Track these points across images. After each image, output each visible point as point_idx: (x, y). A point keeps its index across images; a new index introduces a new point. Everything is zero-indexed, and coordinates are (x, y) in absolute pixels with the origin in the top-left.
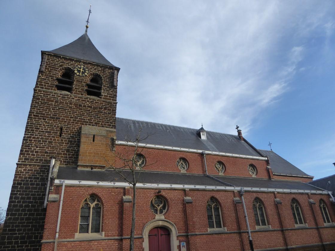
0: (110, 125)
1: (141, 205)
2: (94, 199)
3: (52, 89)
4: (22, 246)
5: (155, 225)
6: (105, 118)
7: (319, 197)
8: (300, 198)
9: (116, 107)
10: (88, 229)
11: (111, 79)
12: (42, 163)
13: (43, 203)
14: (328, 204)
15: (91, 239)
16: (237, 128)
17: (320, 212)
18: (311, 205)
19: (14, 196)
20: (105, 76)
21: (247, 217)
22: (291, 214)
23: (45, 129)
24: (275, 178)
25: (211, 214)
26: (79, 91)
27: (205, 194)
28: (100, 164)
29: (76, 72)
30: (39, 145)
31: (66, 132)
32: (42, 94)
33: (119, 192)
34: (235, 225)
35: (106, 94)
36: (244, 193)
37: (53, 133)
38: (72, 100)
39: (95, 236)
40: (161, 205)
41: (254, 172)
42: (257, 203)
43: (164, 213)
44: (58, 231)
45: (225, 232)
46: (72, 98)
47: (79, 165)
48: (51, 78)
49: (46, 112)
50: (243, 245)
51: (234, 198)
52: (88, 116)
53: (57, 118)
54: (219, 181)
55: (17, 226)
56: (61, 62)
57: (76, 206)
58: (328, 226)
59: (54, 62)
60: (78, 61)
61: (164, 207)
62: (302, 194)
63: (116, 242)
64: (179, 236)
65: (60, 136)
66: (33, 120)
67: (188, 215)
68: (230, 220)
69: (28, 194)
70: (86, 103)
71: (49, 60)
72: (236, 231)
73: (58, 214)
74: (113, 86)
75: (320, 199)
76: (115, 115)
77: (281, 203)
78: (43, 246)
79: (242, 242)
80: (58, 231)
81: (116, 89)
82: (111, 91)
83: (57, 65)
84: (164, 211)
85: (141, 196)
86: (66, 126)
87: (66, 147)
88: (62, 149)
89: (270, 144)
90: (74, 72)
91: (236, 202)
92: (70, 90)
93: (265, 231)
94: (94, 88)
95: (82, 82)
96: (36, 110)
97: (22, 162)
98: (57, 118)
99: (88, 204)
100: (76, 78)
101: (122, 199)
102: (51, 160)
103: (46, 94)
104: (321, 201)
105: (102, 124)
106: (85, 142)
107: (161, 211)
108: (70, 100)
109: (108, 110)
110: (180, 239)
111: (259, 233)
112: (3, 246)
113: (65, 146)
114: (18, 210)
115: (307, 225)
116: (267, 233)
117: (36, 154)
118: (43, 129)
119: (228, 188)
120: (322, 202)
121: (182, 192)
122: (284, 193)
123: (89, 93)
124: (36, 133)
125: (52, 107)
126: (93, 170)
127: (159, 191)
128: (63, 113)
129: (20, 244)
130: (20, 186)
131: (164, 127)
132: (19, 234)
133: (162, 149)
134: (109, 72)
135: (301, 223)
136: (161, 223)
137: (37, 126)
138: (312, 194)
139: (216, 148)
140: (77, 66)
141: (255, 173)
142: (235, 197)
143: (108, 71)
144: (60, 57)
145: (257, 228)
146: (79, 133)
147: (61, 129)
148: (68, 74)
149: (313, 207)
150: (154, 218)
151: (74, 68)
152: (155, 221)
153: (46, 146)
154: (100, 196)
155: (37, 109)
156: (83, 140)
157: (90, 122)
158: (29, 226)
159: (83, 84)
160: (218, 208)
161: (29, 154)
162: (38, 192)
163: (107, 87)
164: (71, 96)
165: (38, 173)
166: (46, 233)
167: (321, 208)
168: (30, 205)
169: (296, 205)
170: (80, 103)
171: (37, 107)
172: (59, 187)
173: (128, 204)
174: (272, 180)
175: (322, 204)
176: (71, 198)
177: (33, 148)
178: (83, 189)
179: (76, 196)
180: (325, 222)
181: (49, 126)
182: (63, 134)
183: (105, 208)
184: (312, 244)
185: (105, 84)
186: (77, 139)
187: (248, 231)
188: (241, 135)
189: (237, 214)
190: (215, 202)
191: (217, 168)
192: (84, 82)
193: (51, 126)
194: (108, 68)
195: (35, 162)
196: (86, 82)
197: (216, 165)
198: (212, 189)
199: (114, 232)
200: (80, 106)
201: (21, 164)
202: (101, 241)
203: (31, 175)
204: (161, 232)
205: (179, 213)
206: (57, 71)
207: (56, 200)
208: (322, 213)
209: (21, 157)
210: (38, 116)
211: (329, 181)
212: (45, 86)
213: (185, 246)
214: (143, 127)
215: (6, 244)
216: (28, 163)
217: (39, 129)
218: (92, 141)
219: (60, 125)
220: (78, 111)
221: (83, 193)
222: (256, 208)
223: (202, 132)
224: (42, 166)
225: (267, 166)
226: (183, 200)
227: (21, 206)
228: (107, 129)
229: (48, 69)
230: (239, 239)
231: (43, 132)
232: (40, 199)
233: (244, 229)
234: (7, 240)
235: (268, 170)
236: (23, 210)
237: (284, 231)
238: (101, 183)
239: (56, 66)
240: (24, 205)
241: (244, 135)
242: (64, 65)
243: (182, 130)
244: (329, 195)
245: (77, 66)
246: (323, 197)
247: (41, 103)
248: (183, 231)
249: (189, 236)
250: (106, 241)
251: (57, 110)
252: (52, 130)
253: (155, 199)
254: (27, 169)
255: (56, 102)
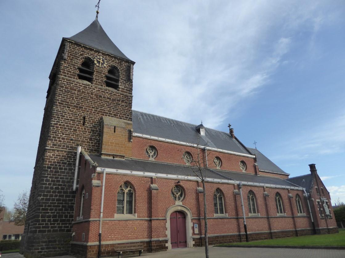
0: (127, 118)
1: (164, 192)
2: (127, 185)
3: (74, 78)
4: (54, 224)
5: (175, 209)
6: (122, 111)
7: (296, 192)
8: (281, 192)
9: (132, 101)
10: (123, 211)
11: (127, 73)
12: (69, 149)
13: (72, 186)
14: (302, 198)
15: (127, 219)
16: (230, 126)
17: (296, 204)
18: (290, 198)
19: (45, 179)
20: (121, 68)
21: (243, 206)
22: (275, 205)
23: (70, 117)
24: (260, 174)
25: (216, 203)
26: (99, 82)
27: (213, 185)
28: (121, 153)
29: (96, 62)
30: (65, 132)
31: (89, 121)
32: (66, 82)
33: (147, 180)
34: (234, 212)
35: (123, 87)
36: (242, 187)
37: (77, 121)
38: (93, 91)
39: (130, 216)
40: (179, 193)
41: (244, 168)
42: (251, 195)
43: (181, 200)
44: (102, 211)
45: (227, 217)
46: (93, 89)
47: (102, 153)
48: (73, 67)
49: (70, 101)
50: (239, 228)
51: (234, 190)
52: (108, 107)
53: (80, 107)
54: (220, 175)
55: (49, 206)
56: (81, 51)
57: (114, 191)
58: (301, 216)
59: (75, 51)
60: (116, 58)
61: (181, 195)
62: (284, 189)
63: (146, 222)
64: (193, 219)
65: (84, 124)
66: (58, 108)
67: (200, 202)
68: (231, 208)
69: (58, 178)
70: (106, 94)
71: (71, 47)
72: (234, 217)
73: (101, 197)
74: (129, 80)
75: (296, 193)
76: (131, 108)
77: (268, 196)
78: (91, 224)
79: (239, 225)
80: (102, 211)
81: (132, 82)
82: (127, 85)
83: (77, 53)
84: (181, 198)
85: (165, 185)
86: (89, 115)
87: (89, 136)
88: (86, 137)
89: (255, 143)
90: (94, 62)
91: (235, 193)
92: (90, 80)
93: (256, 218)
94: (112, 81)
95: (101, 73)
96: (60, 98)
97: (50, 147)
98: (80, 107)
99: (122, 190)
100: (96, 68)
101: (150, 187)
102: (77, 147)
103: (70, 83)
104: (297, 195)
105: (120, 116)
106: (107, 133)
107: (179, 198)
108: (91, 90)
109: (125, 103)
110: (194, 221)
111: (251, 219)
112: (38, 223)
113: (88, 135)
114: (49, 192)
115: (259, 215)
116: (257, 219)
117: (62, 140)
118: (67, 117)
119: (230, 182)
120: (298, 196)
121: (196, 184)
122: (271, 188)
123: (108, 85)
124: (62, 120)
125: (75, 96)
126: (115, 159)
127: (178, 181)
128: (85, 102)
129: (53, 222)
130: (50, 170)
131: (171, 121)
132: (51, 213)
133: (171, 143)
134: (125, 66)
135: (281, 212)
136: (179, 208)
137: (63, 114)
138: (291, 189)
139: (214, 144)
140: (96, 56)
141: (245, 169)
142: (235, 189)
143: (124, 65)
144: (81, 46)
145: (250, 215)
146: (101, 123)
147: (84, 118)
148: (88, 63)
149: (291, 200)
150: (175, 204)
151: (94, 58)
152: (175, 206)
153: (71, 133)
154: (133, 184)
155: (61, 97)
156: (105, 130)
157: (109, 113)
158: (59, 206)
159: (102, 76)
160: (222, 198)
161: (56, 140)
162: (66, 176)
163: (124, 80)
164: (92, 86)
165: (66, 159)
166: (93, 213)
167: (296, 201)
168: (60, 187)
169: (252, 196)
170: (100, 94)
171: (62, 95)
172: (100, 174)
173: (155, 191)
174: (258, 175)
175: (298, 198)
176: (110, 184)
177: (59, 135)
178: (119, 177)
179: (114, 183)
180: (299, 213)
181: (73, 114)
182: (86, 123)
183: (137, 194)
184: (288, 230)
185: (122, 77)
186: (99, 129)
187: (243, 217)
188: (233, 133)
189: (236, 203)
190: (219, 193)
191: (215, 163)
192: (104, 74)
193: (75, 114)
194: (124, 61)
195: (62, 148)
196: (105, 74)
197: (148, 150)
198: (219, 182)
199: (144, 214)
200: (100, 96)
201: (50, 149)
202: (135, 221)
203: (59, 160)
204: (179, 216)
205: (193, 201)
206: (78, 59)
207: (100, 185)
208: (297, 205)
209: (50, 142)
210: (63, 104)
211: (303, 179)
212: (68, 74)
213: (198, 227)
214: (151, 119)
215: (41, 221)
216: (55, 149)
217: (64, 116)
218: (113, 132)
219: (83, 114)
220: (99, 102)
221: (119, 180)
222: (249, 199)
223: (202, 128)
224: (69, 152)
225: (255, 164)
226: (196, 190)
227: (52, 188)
228: (125, 121)
229: (70, 57)
230: (236, 223)
231: (68, 120)
232: (68, 182)
233: (240, 216)
234: (51, 219)
235: (255, 167)
236: (53, 192)
237: (269, 218)
238: (135, 173)
239: (77, 55)
240: (54, 187)
241: (235, 134)
242: (84, 54)
243: (184, 125)
244: (303, 191)
245: (96, 56)
246: (299, 192)
247: (65, 92)
248: (196, 215)
249: (201, 220)
250: (139, 221)
251: (80, 99)
252: (76, 118)
253: (174, 188)
254: (56, 154)
255: (79, 91)
